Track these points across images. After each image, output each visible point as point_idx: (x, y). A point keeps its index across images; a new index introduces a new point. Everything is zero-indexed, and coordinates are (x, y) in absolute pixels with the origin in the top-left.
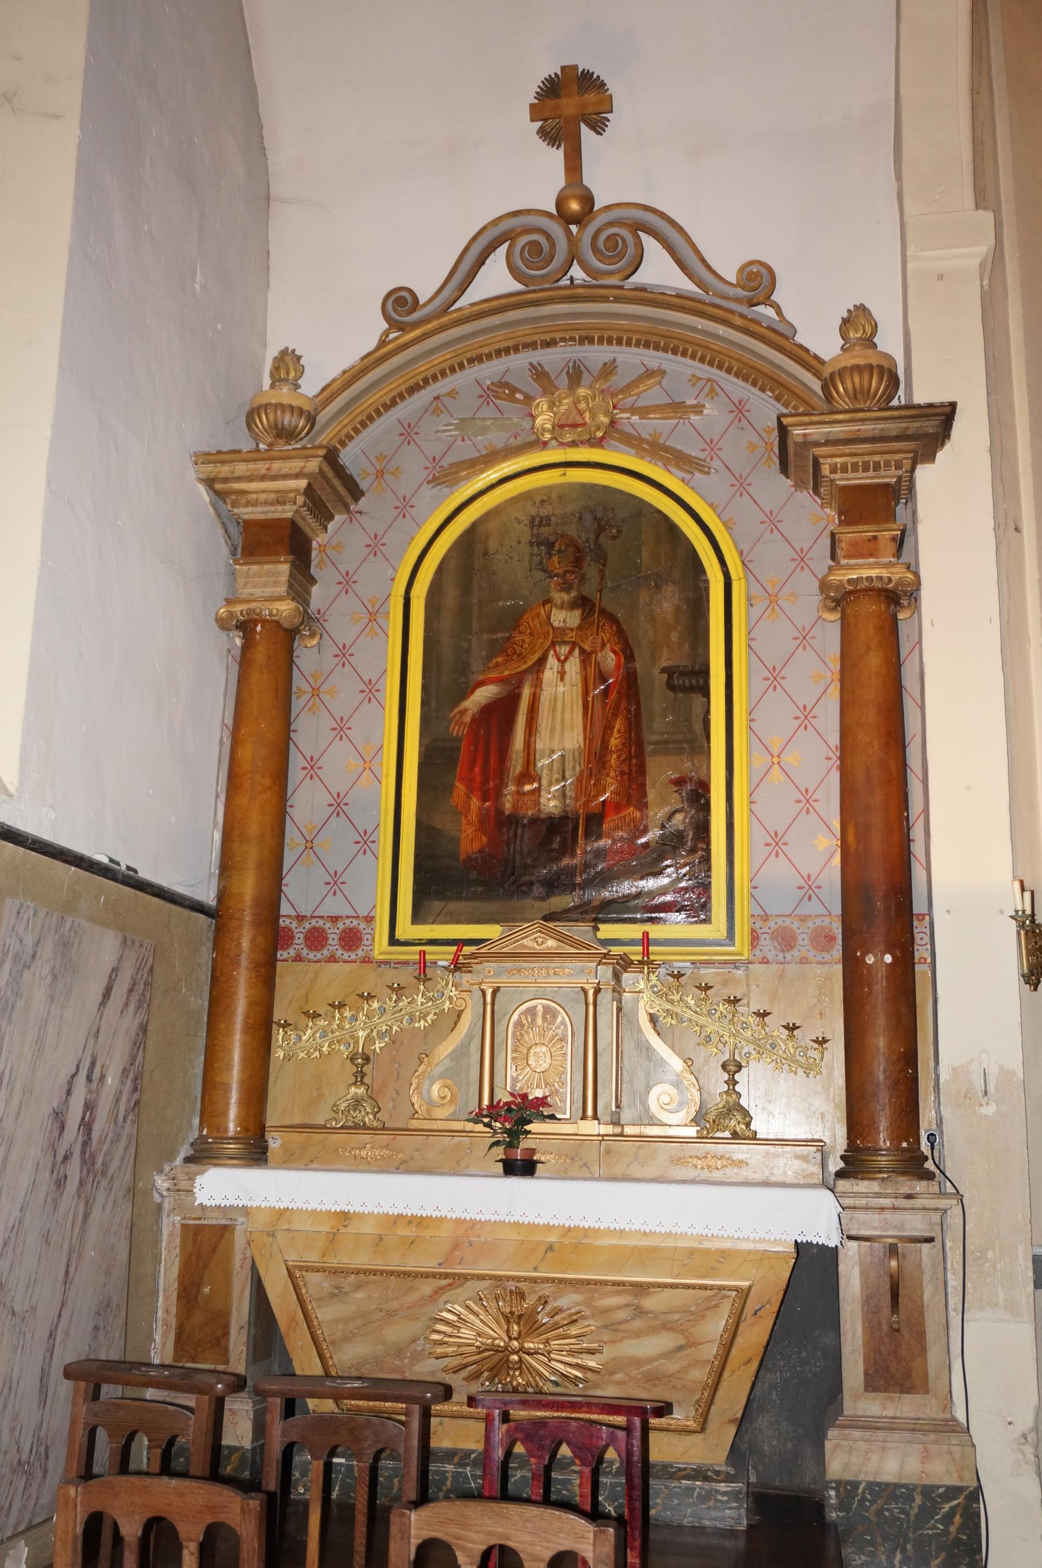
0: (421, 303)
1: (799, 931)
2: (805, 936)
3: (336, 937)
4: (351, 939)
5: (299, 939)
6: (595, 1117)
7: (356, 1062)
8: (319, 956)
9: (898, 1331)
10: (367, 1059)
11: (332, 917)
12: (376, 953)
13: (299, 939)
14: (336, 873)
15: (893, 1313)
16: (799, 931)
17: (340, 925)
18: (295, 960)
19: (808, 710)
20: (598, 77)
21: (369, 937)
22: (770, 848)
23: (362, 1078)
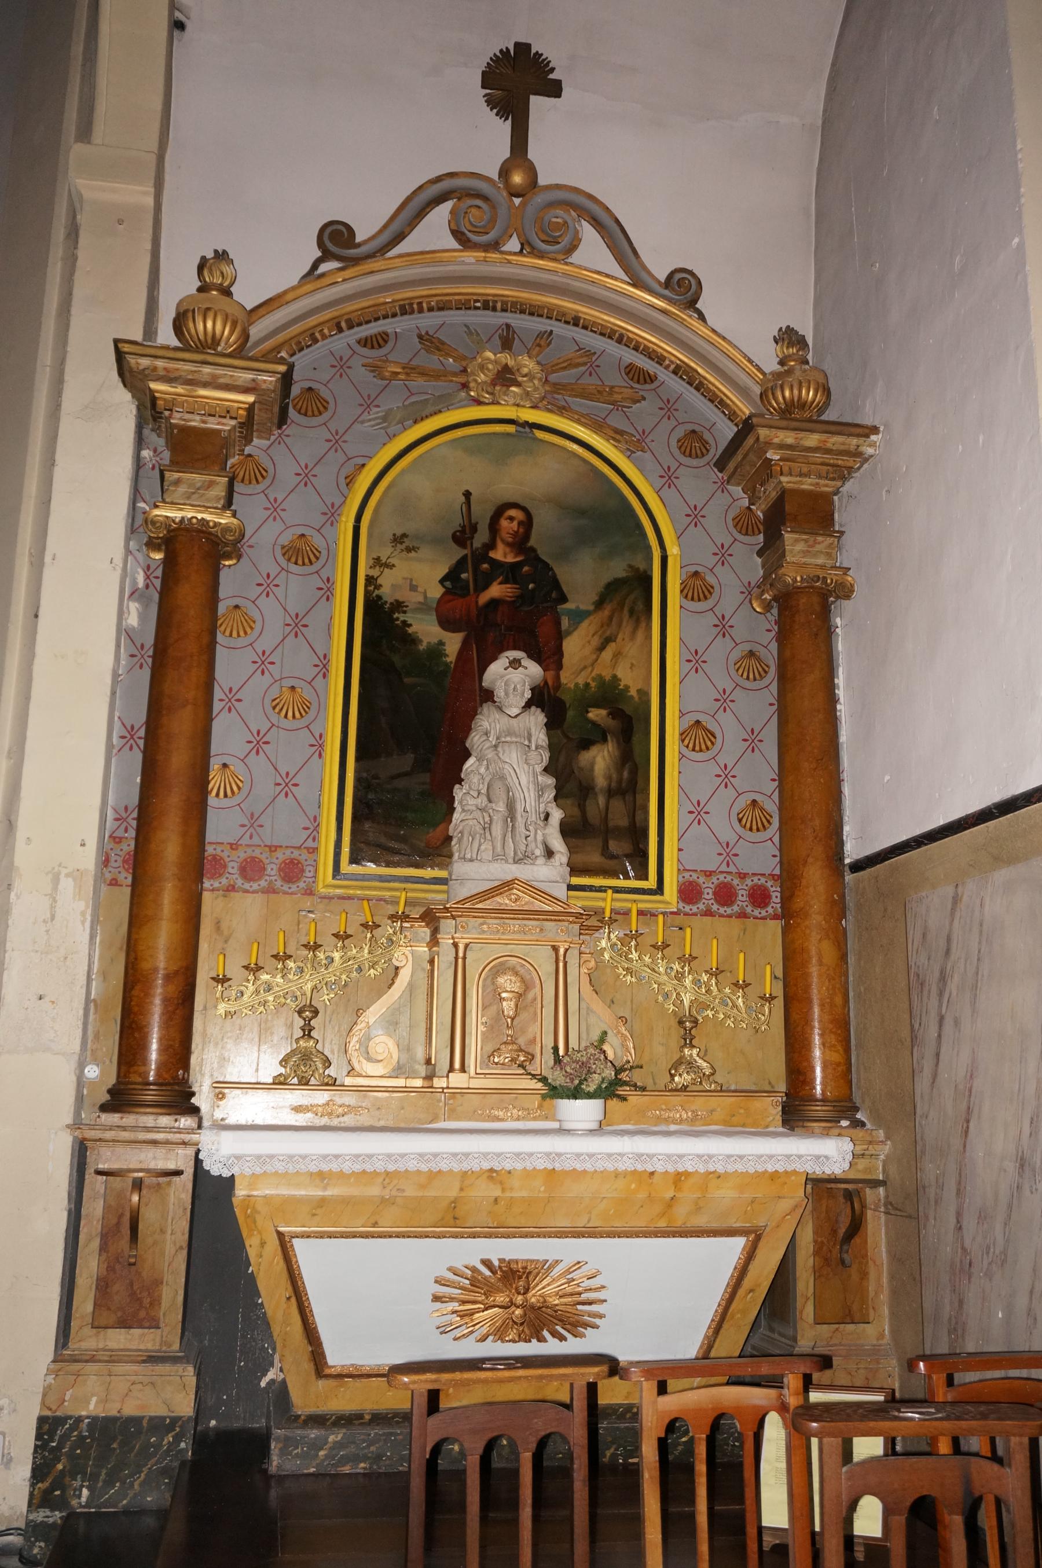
0: (358, 240)
1: (704, 886)
2: (274, 867)
3: (710, 891)
4: (292, 871)
5: (233, 868)
6: (463, 1069)
7: (304, 1015)
8: (695, 909)
9: (134, 1264)
10: (695, 1022)
11: (705, 872)
12: (321, 885)
13: (233, 868)
14: (699, 823)
15: (131, 1248)
16: (772, 889)
17: (749, 882)
18: (305, 894)
19: (727, 694)
20: (491, 110)
21: (311, 868)
22: (294, 781)
23: (310, 1031)
